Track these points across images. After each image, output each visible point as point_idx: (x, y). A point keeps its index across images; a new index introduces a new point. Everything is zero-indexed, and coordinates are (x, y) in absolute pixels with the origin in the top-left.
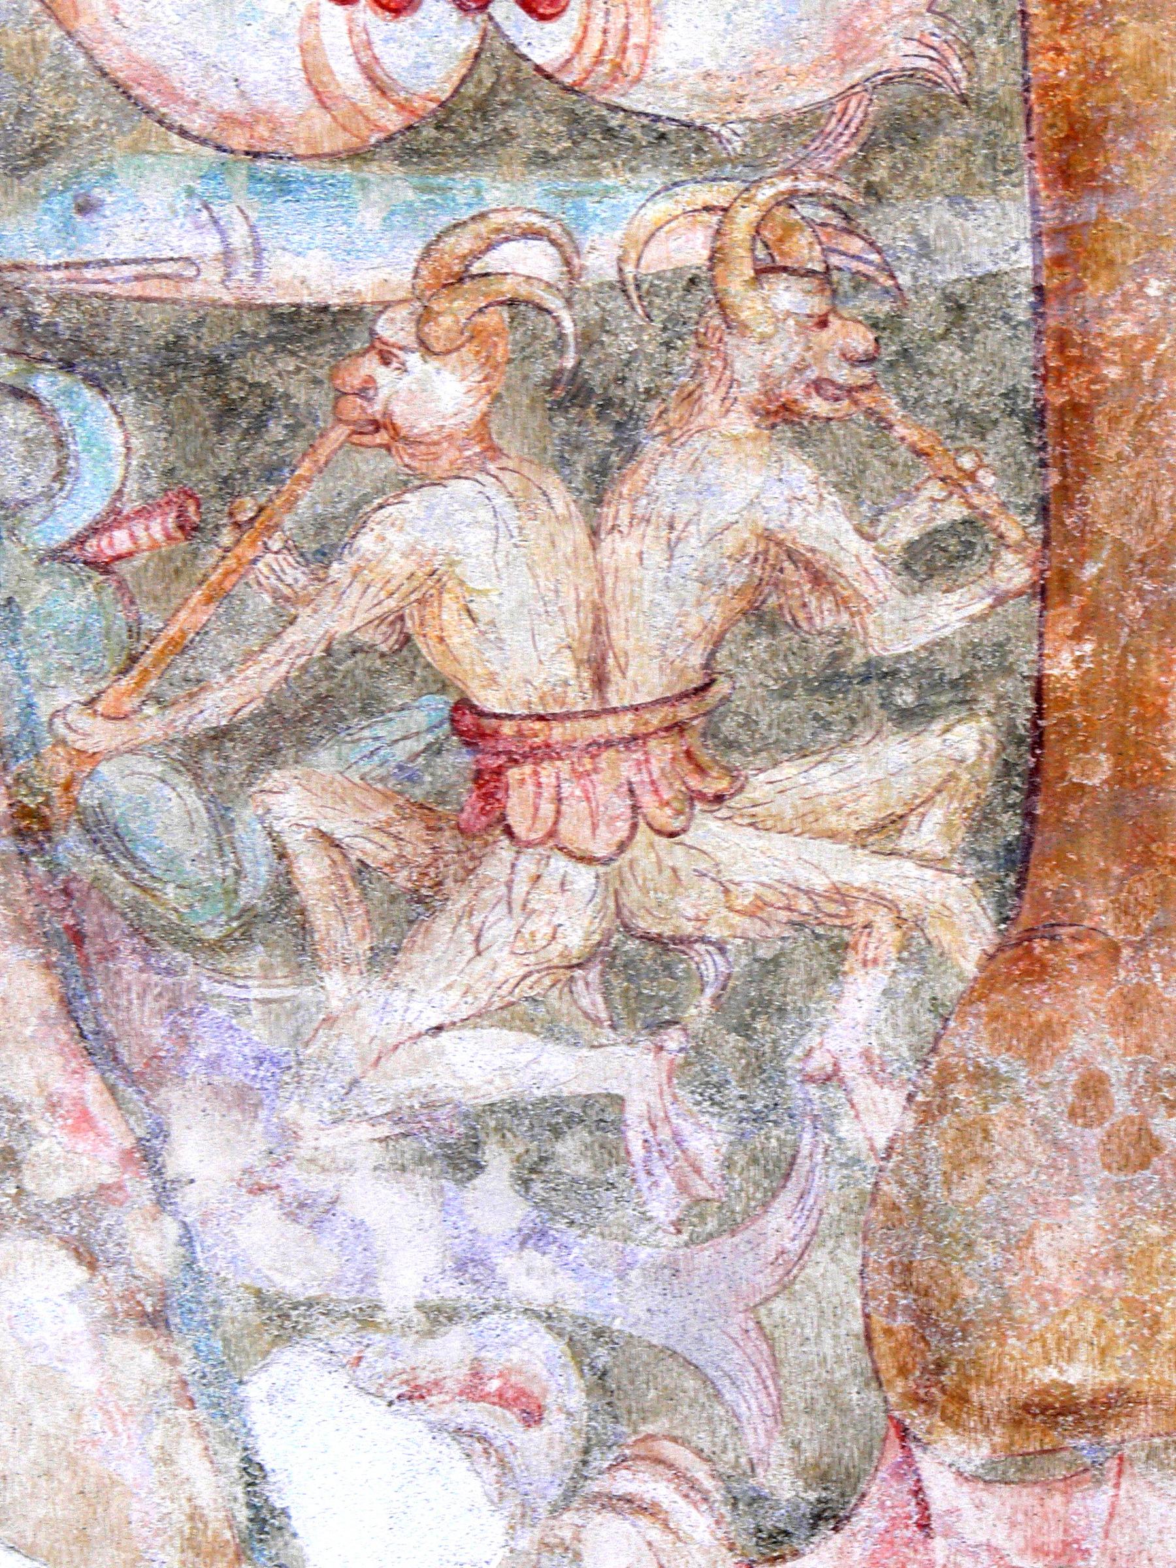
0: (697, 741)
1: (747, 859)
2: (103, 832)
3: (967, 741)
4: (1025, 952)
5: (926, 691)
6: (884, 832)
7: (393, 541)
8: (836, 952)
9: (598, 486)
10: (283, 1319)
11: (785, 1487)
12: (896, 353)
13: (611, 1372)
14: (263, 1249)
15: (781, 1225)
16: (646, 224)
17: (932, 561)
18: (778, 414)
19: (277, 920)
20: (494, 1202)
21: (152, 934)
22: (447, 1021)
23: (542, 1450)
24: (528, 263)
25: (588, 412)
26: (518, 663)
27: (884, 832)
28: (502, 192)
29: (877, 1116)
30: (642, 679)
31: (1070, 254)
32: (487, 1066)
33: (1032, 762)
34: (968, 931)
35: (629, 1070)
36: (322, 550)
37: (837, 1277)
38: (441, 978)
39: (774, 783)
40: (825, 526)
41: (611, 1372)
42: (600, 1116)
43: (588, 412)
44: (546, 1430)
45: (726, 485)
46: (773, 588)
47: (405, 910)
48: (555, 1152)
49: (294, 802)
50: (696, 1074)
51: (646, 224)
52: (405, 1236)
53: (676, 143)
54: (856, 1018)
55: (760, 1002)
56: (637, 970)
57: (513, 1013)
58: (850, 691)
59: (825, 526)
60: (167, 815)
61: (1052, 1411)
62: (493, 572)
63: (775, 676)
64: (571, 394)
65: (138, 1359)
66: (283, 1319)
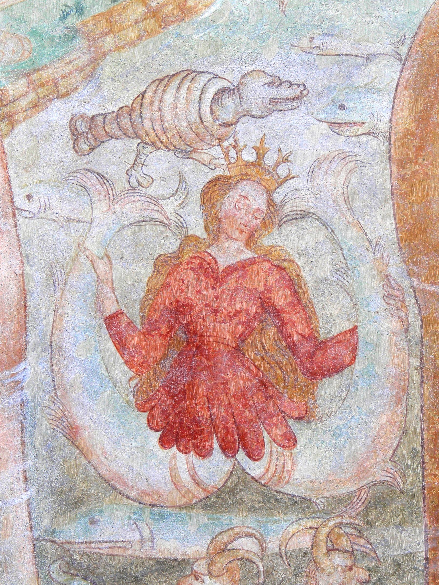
24: (248, 545)
28: (239, 521)
51: (288, 533)
53: (300, 505)
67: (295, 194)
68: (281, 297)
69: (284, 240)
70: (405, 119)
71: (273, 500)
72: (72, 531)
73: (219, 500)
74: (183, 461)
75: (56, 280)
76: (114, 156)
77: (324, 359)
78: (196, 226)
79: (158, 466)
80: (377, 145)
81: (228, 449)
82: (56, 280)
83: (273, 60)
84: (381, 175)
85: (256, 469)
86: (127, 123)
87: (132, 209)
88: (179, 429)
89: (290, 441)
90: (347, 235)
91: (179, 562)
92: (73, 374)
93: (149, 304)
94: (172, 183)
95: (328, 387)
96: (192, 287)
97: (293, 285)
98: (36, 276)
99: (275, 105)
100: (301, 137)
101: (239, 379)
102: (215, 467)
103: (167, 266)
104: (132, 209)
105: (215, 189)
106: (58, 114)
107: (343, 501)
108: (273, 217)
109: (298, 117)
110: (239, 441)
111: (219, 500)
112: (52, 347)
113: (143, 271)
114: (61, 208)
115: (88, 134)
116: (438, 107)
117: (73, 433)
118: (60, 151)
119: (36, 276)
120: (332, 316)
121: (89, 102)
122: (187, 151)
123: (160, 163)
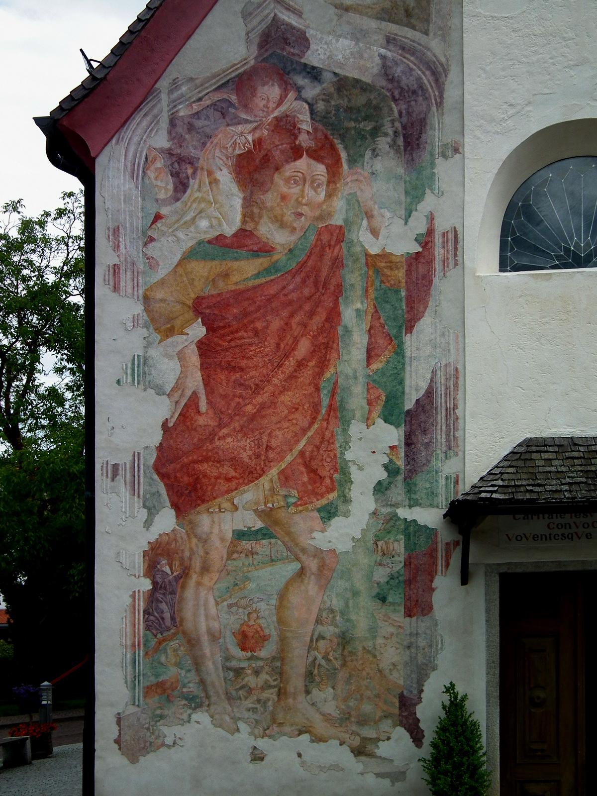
0: (263, 689)
1: (265, 695)
2: (231, 694)
3: (276, 689)
4: (279, 699)
5: (274, 687)
6: (272, 694)
7: (246, 679)
8: (269, 700)
9: (257, 676)
10: (239, 719)
11: (266, 727)
12: (273, 670)
13: (257, 721)
14: (238, 715)
15: (266, 714)
16: (261, 663)
17: (275, 680)
18: (267, 673)
19: (240, 698)
20: (251, 713)
21: (233, 699)
22: (248, 703)
23: (253, 725)
24: (254, 665)
25: (257, 673)
26: (253, 685)
27: (272, 694)
28: (252, 662)
29: (271, 708)
30: (259, 686)
31: (282, 665)
32: (251, 705)
33: (279, 690)
34: (276, 699)
35: (258, 706)
36: (243, 679)
37: (269, 716)
38: (247, 702)
39: (266, 691)
40: (269, 678)
41: (257, 721)
42: (256, 708)
43: (257, 673)
44: (354, 329)
45: (264, 676)
46: (266, 682)
47: (246, 698)
48: (254, 710)
49: (241, 692)
50: (262, 706)
51: (261, 663)
52: (246, 715)
53: (261, 659)
54: (270, 703)
55: (265, 703)
56: (259, 701)
57: (252, 703)
58: (270, 687)
59: (269, 678)
60: (234, 693)
61: (280, 723)
62: (251, 680)
63: (267, 686)
64: (256, 672)
65: (232, 721)
66: (239, 719)
67: (261, 614)
68: (259, 629)
69: (261, 621)
70: (278, 604)
71: (258, 658)
72: (228, 664)
73: (249, 659)
74: (244, 653)
75: (225, 627)
76: (234, 609)
77: (265, 638)
78: (246, 620)
79: (241, 654)
80: (273, 607)
81: (251, 652)
82: (225, 627)
83: (258, 595)
84: (274, 612)
85: (255, 654)
86: (236, 604)
87: (237, 617)
88: (243, 649)
89: (260, 650)
90: (269, 620)
91: (398, 336)
92: (227, 641)
93: (239, 630)
94: (242, 614)
95: (266, 642)
96: (245, 628)
97: (261, 628)
98: (222, 627)
99: (258, 602)
100: (262, 606)
101: (253, 641)
102: (249, 654)
103: (242, 625)
104: (237, 617)
105: (249, 614)
106: (225, 603)
107: (268, 659)
108: (258, 618)
109: (263, 603)
110: (253, 650)
111: (249, 659)
112: (224, 637)
113: (238, 626)
114: (226, 617)
115: (230, 606)
116: (2, 305)
117: (227, 649)
118: (226, 608)
119: (222, 627)
120: (267, 632)
121: (230, 601)
122: (245, 609)
123: (241, 610)
